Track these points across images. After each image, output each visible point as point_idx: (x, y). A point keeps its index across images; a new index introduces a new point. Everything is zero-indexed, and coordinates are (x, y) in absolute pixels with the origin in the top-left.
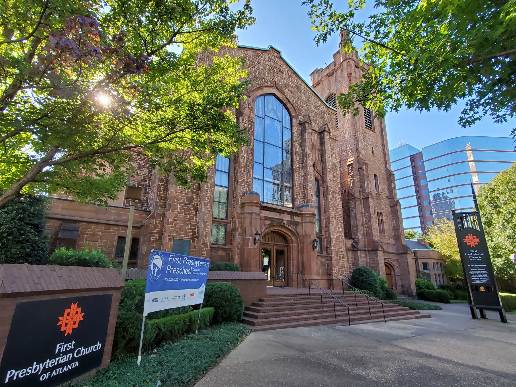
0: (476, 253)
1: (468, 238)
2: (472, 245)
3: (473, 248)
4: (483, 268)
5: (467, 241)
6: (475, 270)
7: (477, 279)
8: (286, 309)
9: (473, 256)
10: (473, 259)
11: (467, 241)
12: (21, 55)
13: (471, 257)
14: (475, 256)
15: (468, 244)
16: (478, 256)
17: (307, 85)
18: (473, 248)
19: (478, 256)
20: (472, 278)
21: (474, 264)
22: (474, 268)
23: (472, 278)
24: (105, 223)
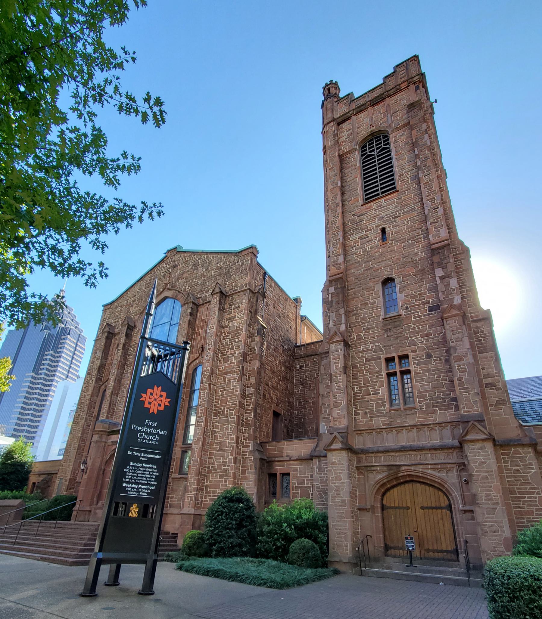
0: (154, 428)
1: (152, 394)
2: (154, 409)
3: (153, 417)
4: (150, 461)
5: (163, 401)
6: (138, 464)
7: (134, 486)
8: (60, 542)
9: (146, 433)
10: (144, 439)
11: (163, 401)
12: (527, 549)
13: (141, 435)
14: (151, 434)
15: (147, 405)
16: (154, 434)
17: (318, 330)
18: (153, 417)
19: (154, 434)
20: (124, 485)
21: (140, 452)
22: (137, 459)
23: (124, 485)
24: (60, 423)
